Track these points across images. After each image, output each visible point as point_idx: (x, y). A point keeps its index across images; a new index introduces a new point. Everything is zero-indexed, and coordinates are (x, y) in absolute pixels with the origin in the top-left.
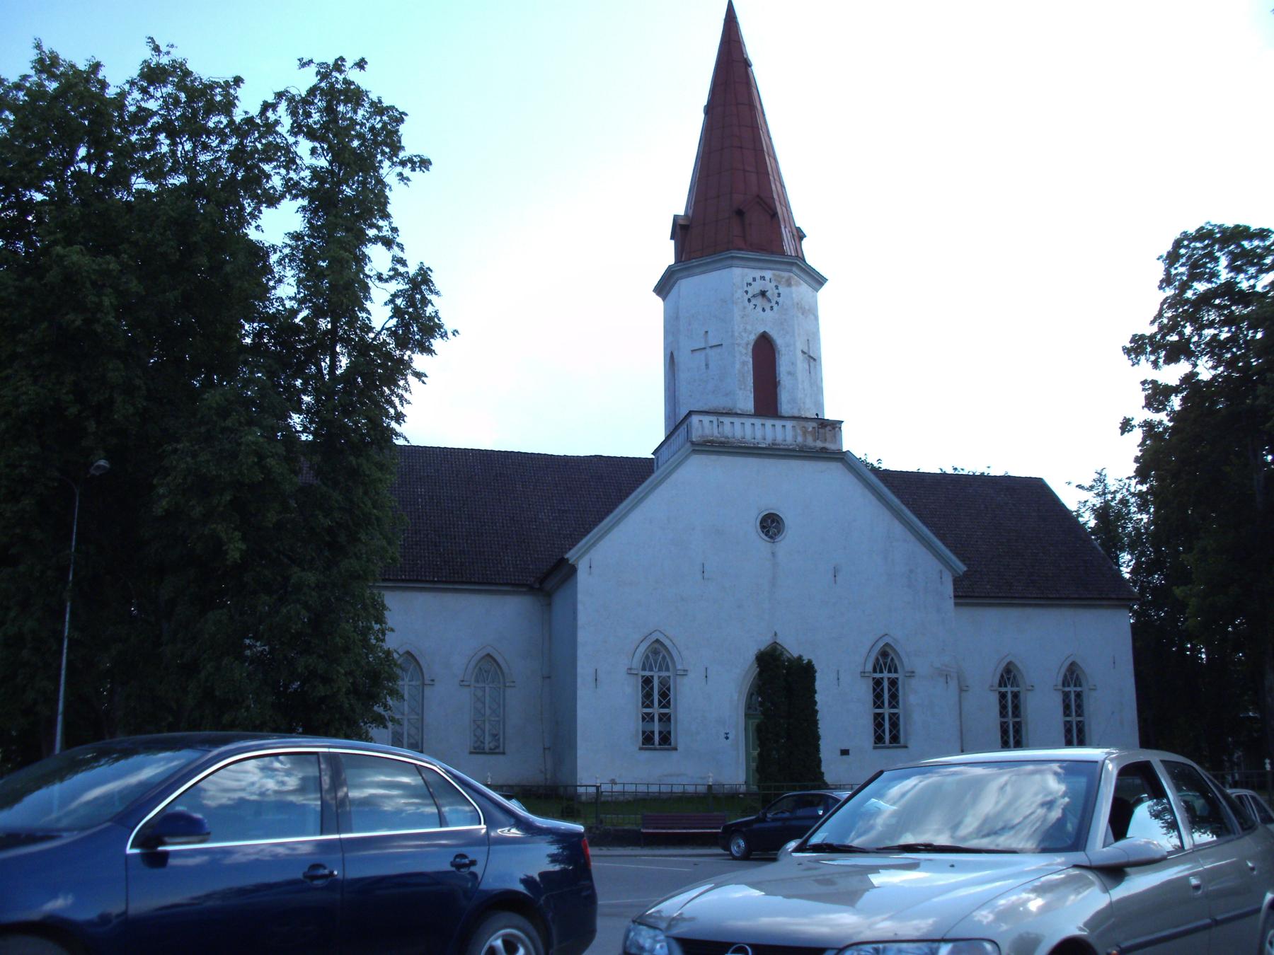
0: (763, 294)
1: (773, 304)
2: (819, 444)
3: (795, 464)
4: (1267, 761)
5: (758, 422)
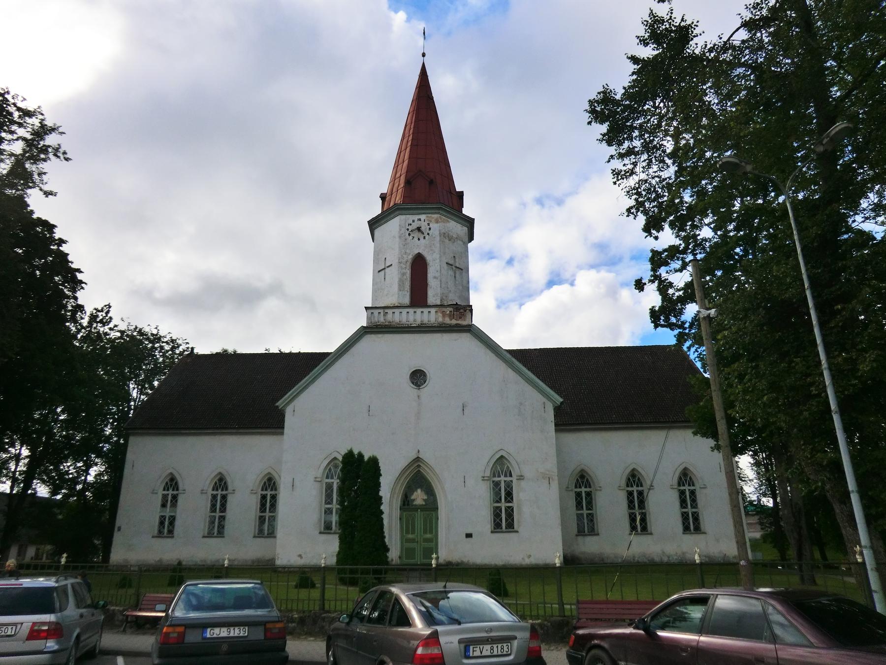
0: (419, 229)
1: (426, 234)
2: (454, 322)
3: (437, 336)
4: (65, 555)
5: (411, 311)
